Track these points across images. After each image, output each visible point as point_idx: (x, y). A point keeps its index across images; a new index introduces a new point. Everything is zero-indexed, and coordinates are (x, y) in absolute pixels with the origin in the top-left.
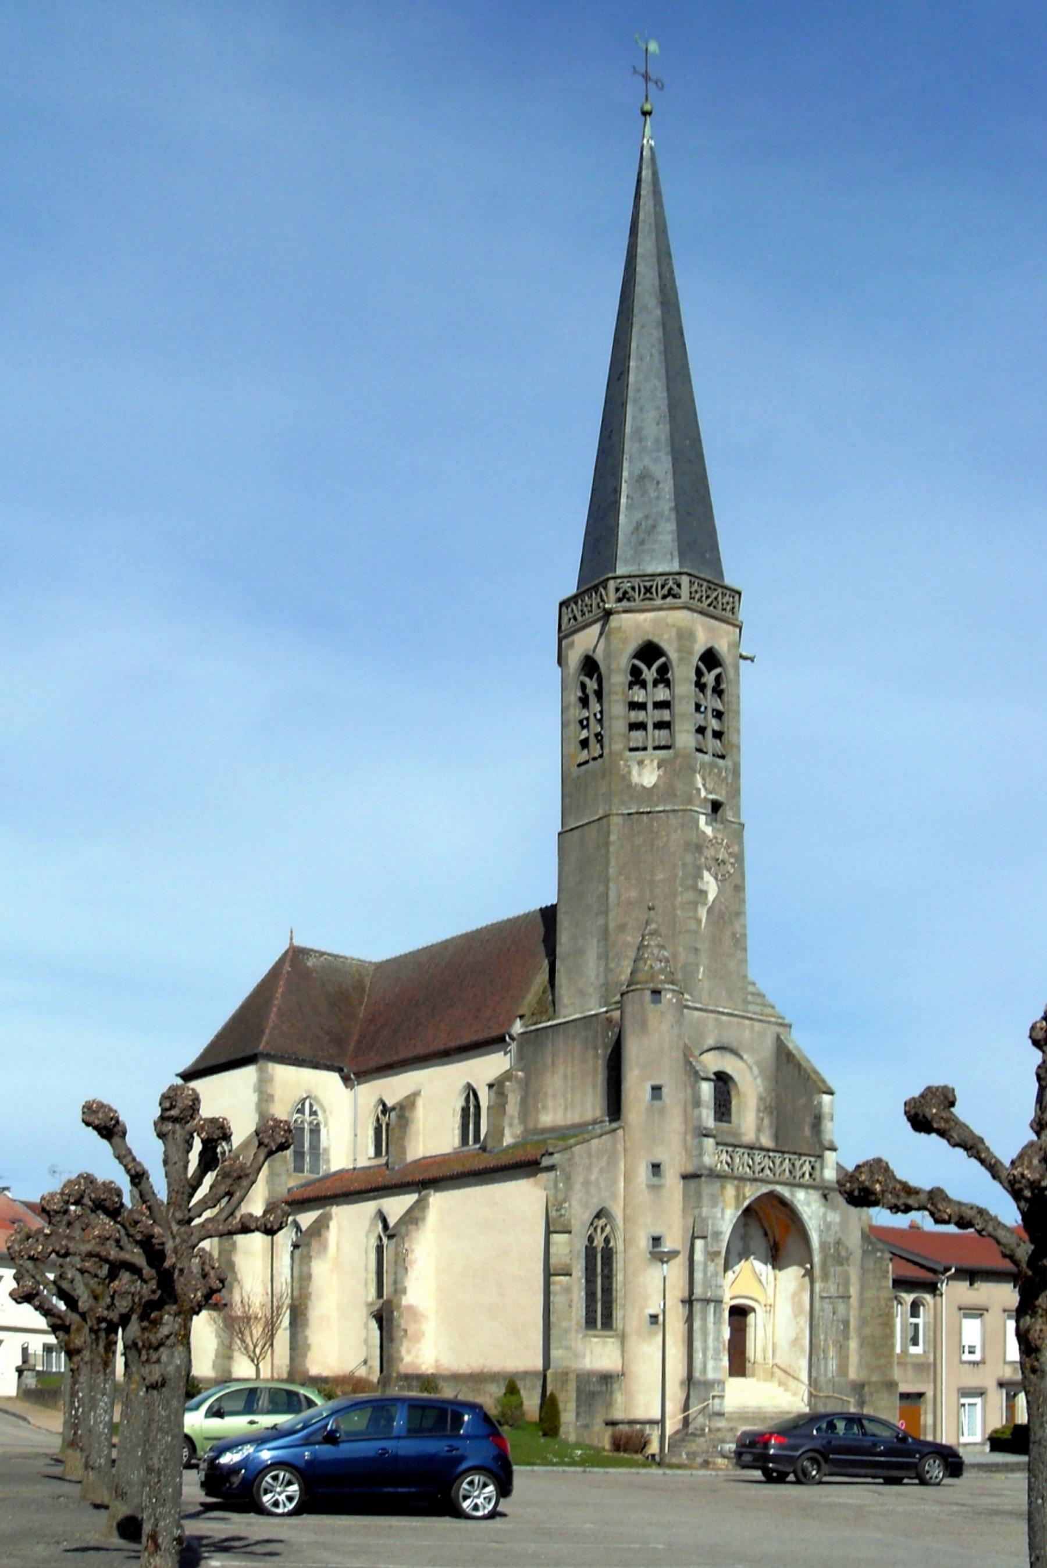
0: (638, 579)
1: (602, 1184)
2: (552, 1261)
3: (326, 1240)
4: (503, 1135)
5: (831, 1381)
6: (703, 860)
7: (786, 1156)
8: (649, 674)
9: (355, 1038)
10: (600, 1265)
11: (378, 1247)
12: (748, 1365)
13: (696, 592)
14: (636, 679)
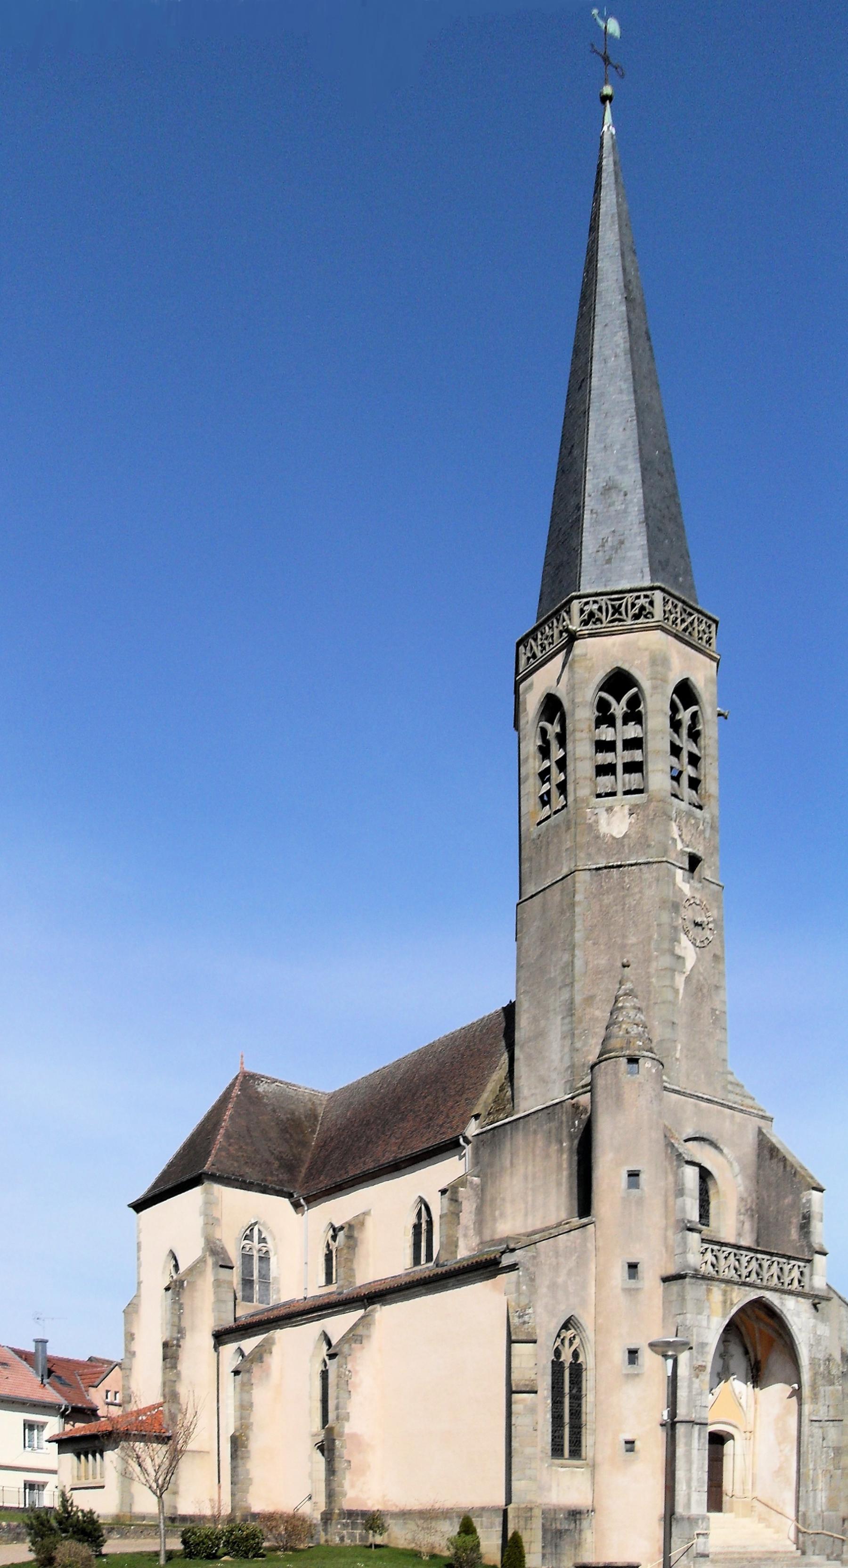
0: (604, 597)
1: (571, 1289)
2: (514, 1376)
3: (269, 1368)
4: (457, 1246)
5: (820, 1515)
6: (680, 921)
7: (774, 1259)
8: (618, 709)
9: (306, 1165)
10: (568, 1382)
11: (323, 1372)
12: (725, 1499)
13: (670, 612)
14: (605, 717)
